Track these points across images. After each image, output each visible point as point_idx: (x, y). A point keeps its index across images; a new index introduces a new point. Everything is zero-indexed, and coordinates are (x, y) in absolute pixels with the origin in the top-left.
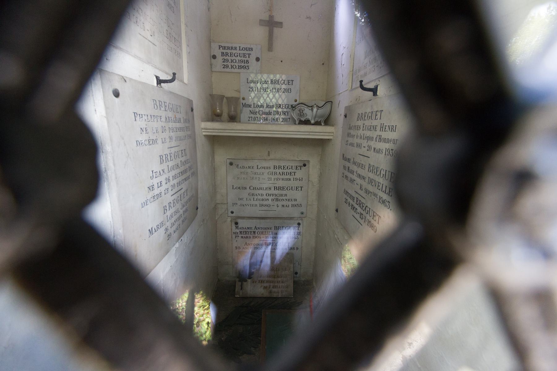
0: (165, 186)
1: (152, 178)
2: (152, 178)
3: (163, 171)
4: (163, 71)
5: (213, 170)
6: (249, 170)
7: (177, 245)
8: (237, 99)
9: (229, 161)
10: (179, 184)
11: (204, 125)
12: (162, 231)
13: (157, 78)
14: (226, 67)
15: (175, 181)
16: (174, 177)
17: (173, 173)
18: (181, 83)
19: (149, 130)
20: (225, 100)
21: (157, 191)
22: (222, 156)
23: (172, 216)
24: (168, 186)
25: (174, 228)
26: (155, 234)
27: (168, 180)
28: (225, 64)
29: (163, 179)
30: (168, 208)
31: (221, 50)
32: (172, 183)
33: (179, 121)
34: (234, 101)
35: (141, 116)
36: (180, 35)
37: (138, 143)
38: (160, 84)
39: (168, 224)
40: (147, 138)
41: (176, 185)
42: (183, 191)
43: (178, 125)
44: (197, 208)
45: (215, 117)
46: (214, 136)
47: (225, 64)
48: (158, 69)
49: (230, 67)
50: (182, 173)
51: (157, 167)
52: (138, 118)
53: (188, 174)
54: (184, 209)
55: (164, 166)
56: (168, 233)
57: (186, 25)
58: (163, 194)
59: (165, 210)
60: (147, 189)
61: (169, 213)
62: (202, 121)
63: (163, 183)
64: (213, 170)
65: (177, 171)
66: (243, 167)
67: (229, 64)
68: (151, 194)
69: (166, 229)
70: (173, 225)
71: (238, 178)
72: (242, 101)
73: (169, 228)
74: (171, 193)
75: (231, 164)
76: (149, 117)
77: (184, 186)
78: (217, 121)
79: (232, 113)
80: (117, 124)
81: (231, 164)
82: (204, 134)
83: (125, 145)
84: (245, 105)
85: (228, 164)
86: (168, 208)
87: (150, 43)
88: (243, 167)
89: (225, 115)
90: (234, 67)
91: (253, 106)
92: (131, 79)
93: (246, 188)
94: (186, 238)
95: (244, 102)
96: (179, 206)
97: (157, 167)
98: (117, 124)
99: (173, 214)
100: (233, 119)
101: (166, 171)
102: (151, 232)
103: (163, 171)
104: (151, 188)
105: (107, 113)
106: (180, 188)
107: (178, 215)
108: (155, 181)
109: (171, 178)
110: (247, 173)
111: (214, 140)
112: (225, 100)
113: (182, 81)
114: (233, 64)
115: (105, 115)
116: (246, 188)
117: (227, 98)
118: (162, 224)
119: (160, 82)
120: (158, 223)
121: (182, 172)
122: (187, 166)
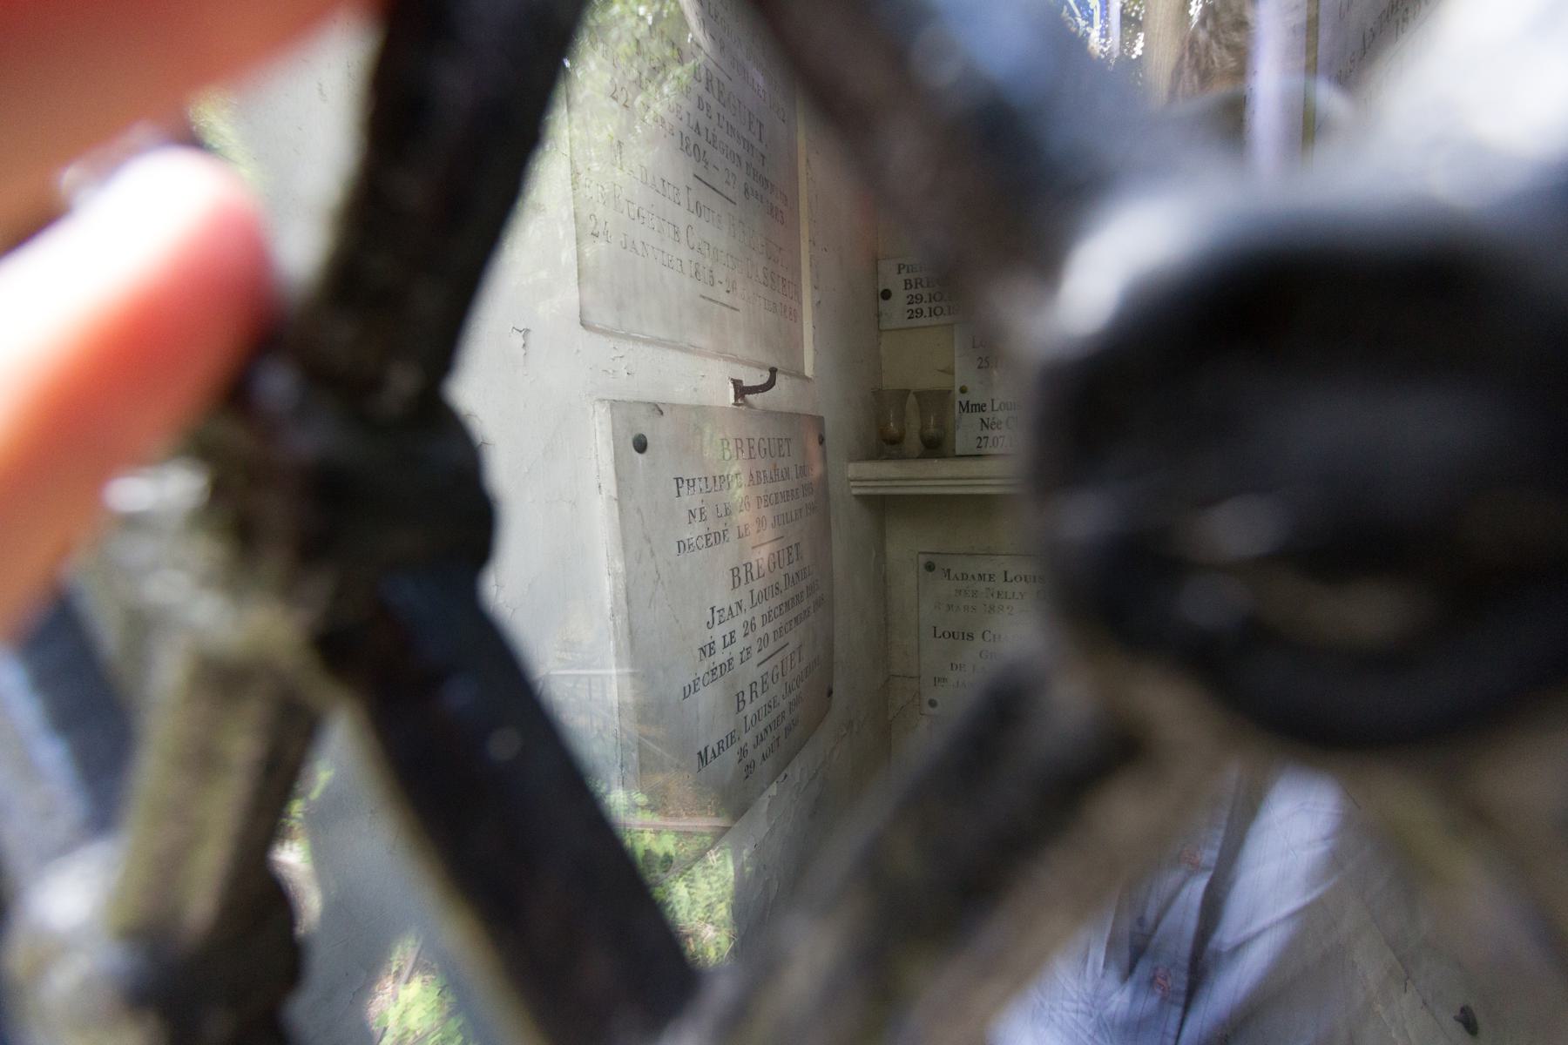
0: (741, 643)
1: (710, 625)
2: (710, 625)
3: (739, 604)
4: (749, 363)
5: (881, 584)
6: (982, 586)
7: (773, 790)
8: (943, 396)
9: (923, 559)
10: (779, 633)
11: (853, 470)
12: (731, 754)
13: (737, 384)
14: (914, 314)
15: (769, 628)
16: (767, 618)
17: (764, 608)
18: (797, 381)
19: (708, 513)
20: (912, 399)
21: (721, 657)
22: (906, 546)
23: (757, 717)
24: (751, 641)
25: (764, 747)
26: (714, 764)
27: (750, 626)
28: (914, 307)
29: (737, 624)
30: (747, 697)
31: (904, 275)
32: (760, 632)
33: (786, 475)
34: (936, 401)
35: (691, 483)
36: (797, 270)
37: (682, 546)
38: (742, 396)
39: (748, 738)
40: (703, 531)
41: (771, 636)
42: (788, 650)
43: (782, 486)
44: (830, 693)
45: (885, 445)
46: (883, 497)
47: (914, 307)
48: (630, 625)
49: (926, 312)
50: (787, 605)
51: (722, 596)
52: (684, 490)
53: (804, 605)
54: (793, 696)
55: (743, 594)
56: (747, 760)
57: (813, 242)
58: (736, 662)
59: (740, 700)
60: (697, 653)
61: (749, 710)
62: (851, 461)
63: (739, 636)
64: (881, 584)
65: (775, 602)
66: (964, 576)
67: (925, 307)
68: (707, 664)
69: (743, 752)
70: (760, 739)
71: (950, 607)
72: (959, 397)
73: (749, 748)
74: (756, 657)
75: (930, 567)
76: (711, 481)
77: (793, 638)
78: (890, 458)
79: (932, 431)
80: (639, 510)
81: (930, 567)
82: (855, 491)
83: (653, 554)
84: (967, 407)
85: (922, 567)
86: (747, 697)
87: (725, 309)
88: (964, 576)
89: (913, 442)
90: (938, 311)
91: (989, 408)
92: (673, 406)
93: (971, 636)
94: (798, 770)
95: (964, 398)
96: (776, 689)
97: (722, 596)
98: (639, 510)
99: (762, 712)
100: (935, 447)
101: (746, 604)
102: (703, 758)
103: (739, 604)
104: (707, 650)
105: (619, 491)
106: (781, 642)
107: (775, 713)
108: (719, 632)
109: (758, 622)
110: (975, 594)
111: (882, 508)
112: (912, 399)
113: (800, 375)
114: (933, 305)
115: (614, 495)
116: (971, 636)
117: (918, 394)
118: (732, 738)
119: (741, 391)
120: (720, 734)
121: (787, 604)
122: (803, 584)
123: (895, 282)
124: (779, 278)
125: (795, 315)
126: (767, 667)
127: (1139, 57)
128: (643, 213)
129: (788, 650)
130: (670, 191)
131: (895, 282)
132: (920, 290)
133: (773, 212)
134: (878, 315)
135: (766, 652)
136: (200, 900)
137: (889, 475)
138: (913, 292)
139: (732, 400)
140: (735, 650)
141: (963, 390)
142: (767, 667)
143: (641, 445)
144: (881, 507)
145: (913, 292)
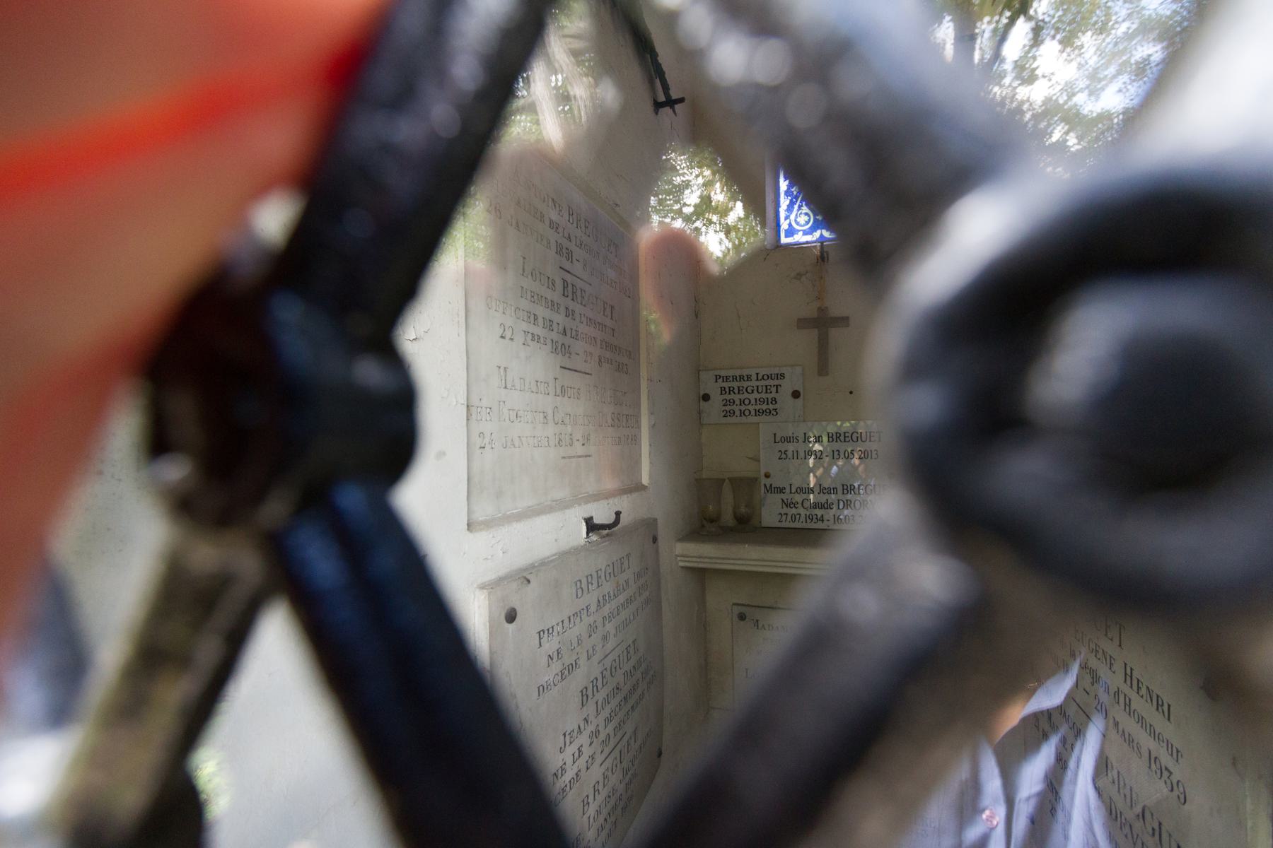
0: (587, 752)
3: (586, 720)
8: (753, 482)
9: (737, 610)
11: (680, 548)
17: (606, 713)
23: (598, 812)
28: (728, 408)
31: (720, 383)
34: (746, 485)
35: (550, 631)
42: (626, 739)
44: (660, 754)
47: (728, 408)
49: (738, 413)
55: (591, 709)
57: (650, 380)
62: (680, 540)
67: (736, 408)
72: (763, 481)
74: (599, 759)
75: (742, 617)
79: (743, 510)
81: (742, 617)
82: (681, 564)
91: (788, 490)
95: (768, 482)
106: (619, 735)
114: (743, 408)
123: (713, 388)
124: (623, 420)
125: (635, 440)
126: (609, 761)
127: (939, 20)
128: (520, 413)
129: (626, 739)
130: (542, 387)
131: (713, 388)
132: (732, 396)
133: (620, 368)
134: (700, 413)
135: (607, 750)
136: (130, 797)
137: (707, 553)
138: (728, 397)
139: (585, 535)
140: (582, 762)
141: (767, 476)
142: (608, 763)
143: (511, 617)
144: (701, 575)
145: (728, 397)
